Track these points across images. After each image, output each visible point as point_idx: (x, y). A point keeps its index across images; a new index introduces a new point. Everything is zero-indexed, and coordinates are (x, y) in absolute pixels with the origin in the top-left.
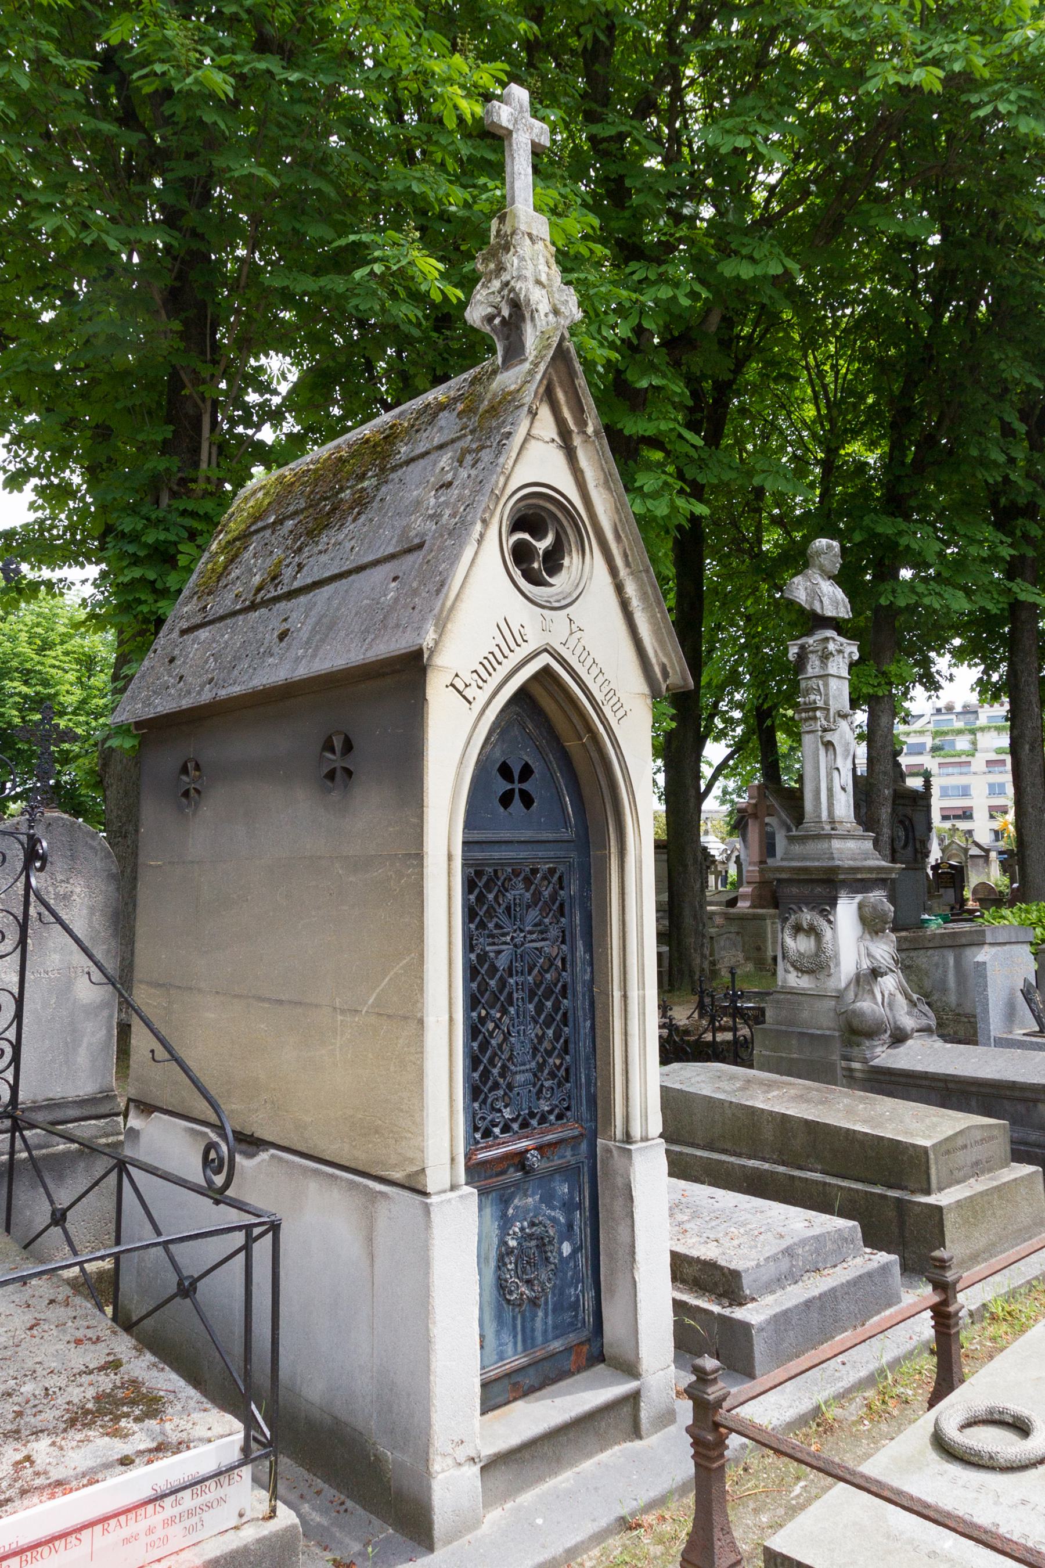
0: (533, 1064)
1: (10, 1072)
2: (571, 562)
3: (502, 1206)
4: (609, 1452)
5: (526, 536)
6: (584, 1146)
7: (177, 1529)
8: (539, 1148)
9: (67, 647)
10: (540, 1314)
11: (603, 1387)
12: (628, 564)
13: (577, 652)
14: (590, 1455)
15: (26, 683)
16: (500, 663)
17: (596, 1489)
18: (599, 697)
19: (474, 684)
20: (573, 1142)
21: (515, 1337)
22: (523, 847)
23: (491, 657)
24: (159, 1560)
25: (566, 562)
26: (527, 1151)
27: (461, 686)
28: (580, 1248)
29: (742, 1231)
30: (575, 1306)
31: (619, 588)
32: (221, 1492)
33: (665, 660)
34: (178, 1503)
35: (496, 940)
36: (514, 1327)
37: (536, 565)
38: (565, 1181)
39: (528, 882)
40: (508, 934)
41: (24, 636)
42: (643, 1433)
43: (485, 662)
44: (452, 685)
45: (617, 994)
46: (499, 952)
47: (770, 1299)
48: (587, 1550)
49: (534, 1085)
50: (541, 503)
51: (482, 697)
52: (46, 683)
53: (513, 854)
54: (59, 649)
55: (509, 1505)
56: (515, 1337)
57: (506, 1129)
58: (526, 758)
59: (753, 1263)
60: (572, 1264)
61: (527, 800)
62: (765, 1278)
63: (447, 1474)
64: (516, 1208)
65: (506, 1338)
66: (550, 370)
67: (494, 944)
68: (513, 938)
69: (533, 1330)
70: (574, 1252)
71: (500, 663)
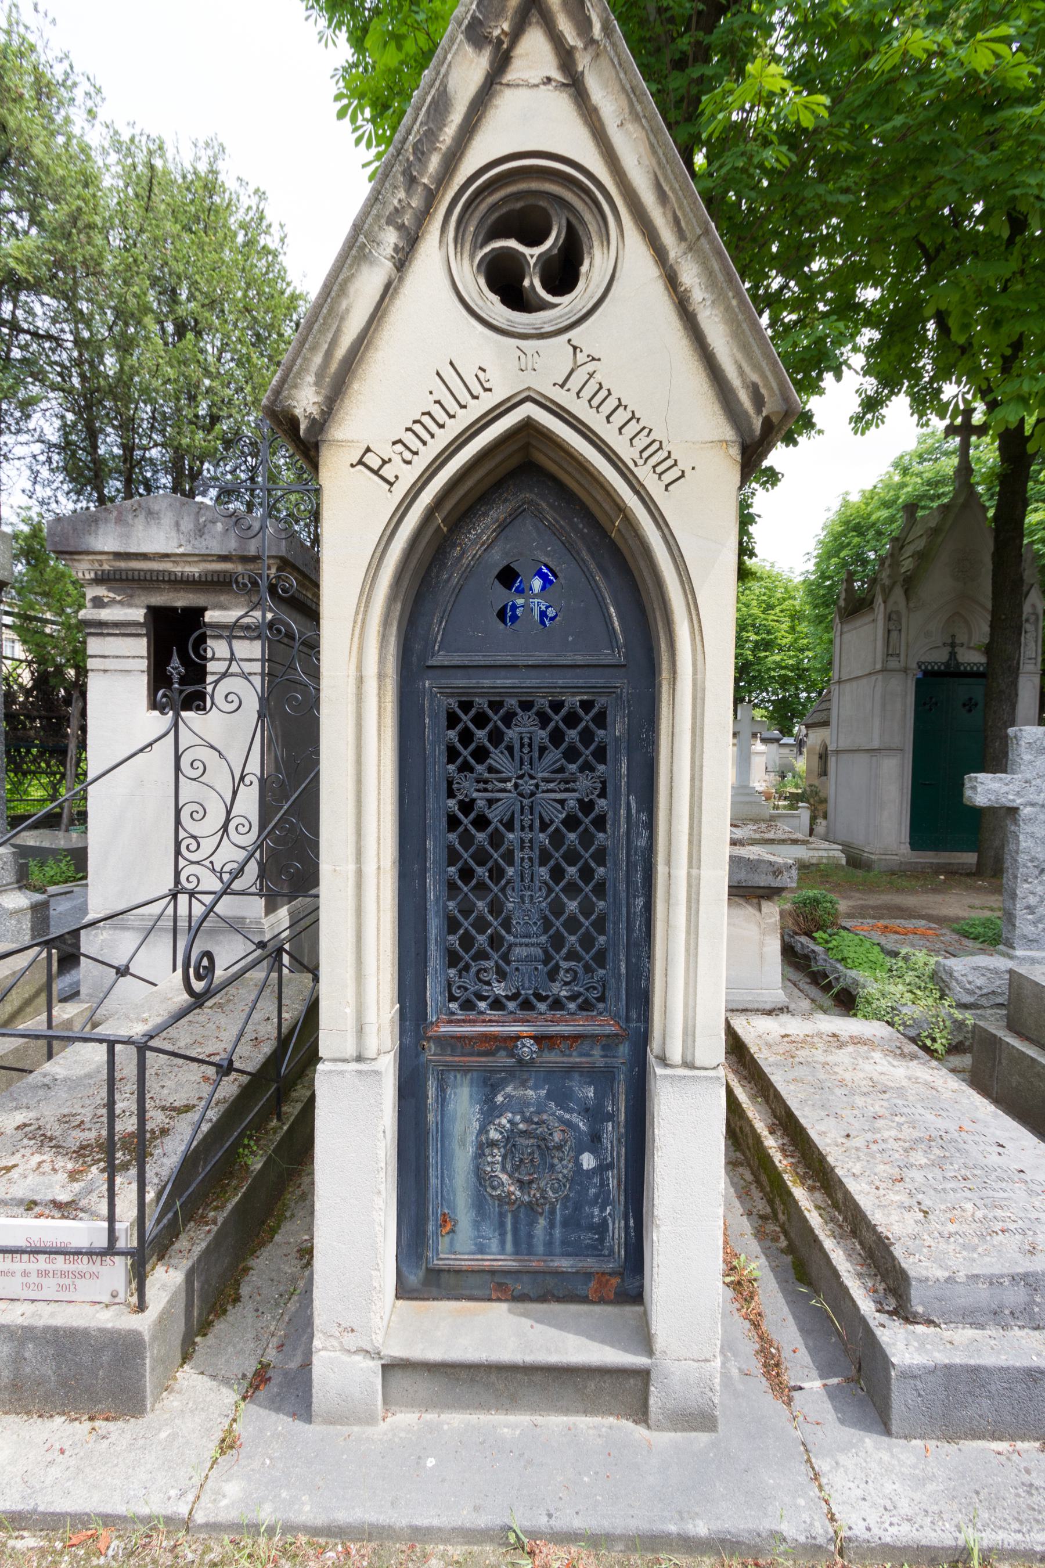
0: (543, 939)
1: (181, 865)
2: (595, 268)
3: (487, 1090)
4: (597, 1420)
5: (512, 243)
6: (624, 1050)
7: (50, 1283)
8: (538, 1039)
9: (784, 607)
10: (542, 1222)
11: (603, 1342)
12: (681, 236)
14: (567, 1411)
15: (757, 634)
17: (530, 1462)
18: (627, 453)
19: (396, 459)
20: (609, 1042)
21: (503, 1235)
22: (533, 672)
23: (426, 420)
24: (33, 1301)
26: (518, 1038)
28: (610, 1166)
29: (979, 1214)
30: (602, 1228)
31: (671, 280)
32: (94, 1268)
33: (755, 377)
34: (51, 1262)
35: (489, 786)
36: (502, 1225)
38: (590, 1084)
39: (544, 720)
40: (509, 780)
41: (754, 603)
43: (417, 428)
44: (361, 462)
46: (490, 802)
47: (965, 1334)
48: (447, 1541)
49: (545, 963)
51: (409, 475)
52: (769, 633)
53: (516, 682)
54: (778, 609)
55: (430, 1417)
56: (503, 1235)
57: (497, 1004)
59: (942, 1274)
60: (596, 1180)
62: (961, 1302)
63: (332, 1354)
64: (508, 1096)
65: (487, 1230)
67: (486, 790)
68: (516, 786)
69: (530, 1236)
70: (602, 1168)
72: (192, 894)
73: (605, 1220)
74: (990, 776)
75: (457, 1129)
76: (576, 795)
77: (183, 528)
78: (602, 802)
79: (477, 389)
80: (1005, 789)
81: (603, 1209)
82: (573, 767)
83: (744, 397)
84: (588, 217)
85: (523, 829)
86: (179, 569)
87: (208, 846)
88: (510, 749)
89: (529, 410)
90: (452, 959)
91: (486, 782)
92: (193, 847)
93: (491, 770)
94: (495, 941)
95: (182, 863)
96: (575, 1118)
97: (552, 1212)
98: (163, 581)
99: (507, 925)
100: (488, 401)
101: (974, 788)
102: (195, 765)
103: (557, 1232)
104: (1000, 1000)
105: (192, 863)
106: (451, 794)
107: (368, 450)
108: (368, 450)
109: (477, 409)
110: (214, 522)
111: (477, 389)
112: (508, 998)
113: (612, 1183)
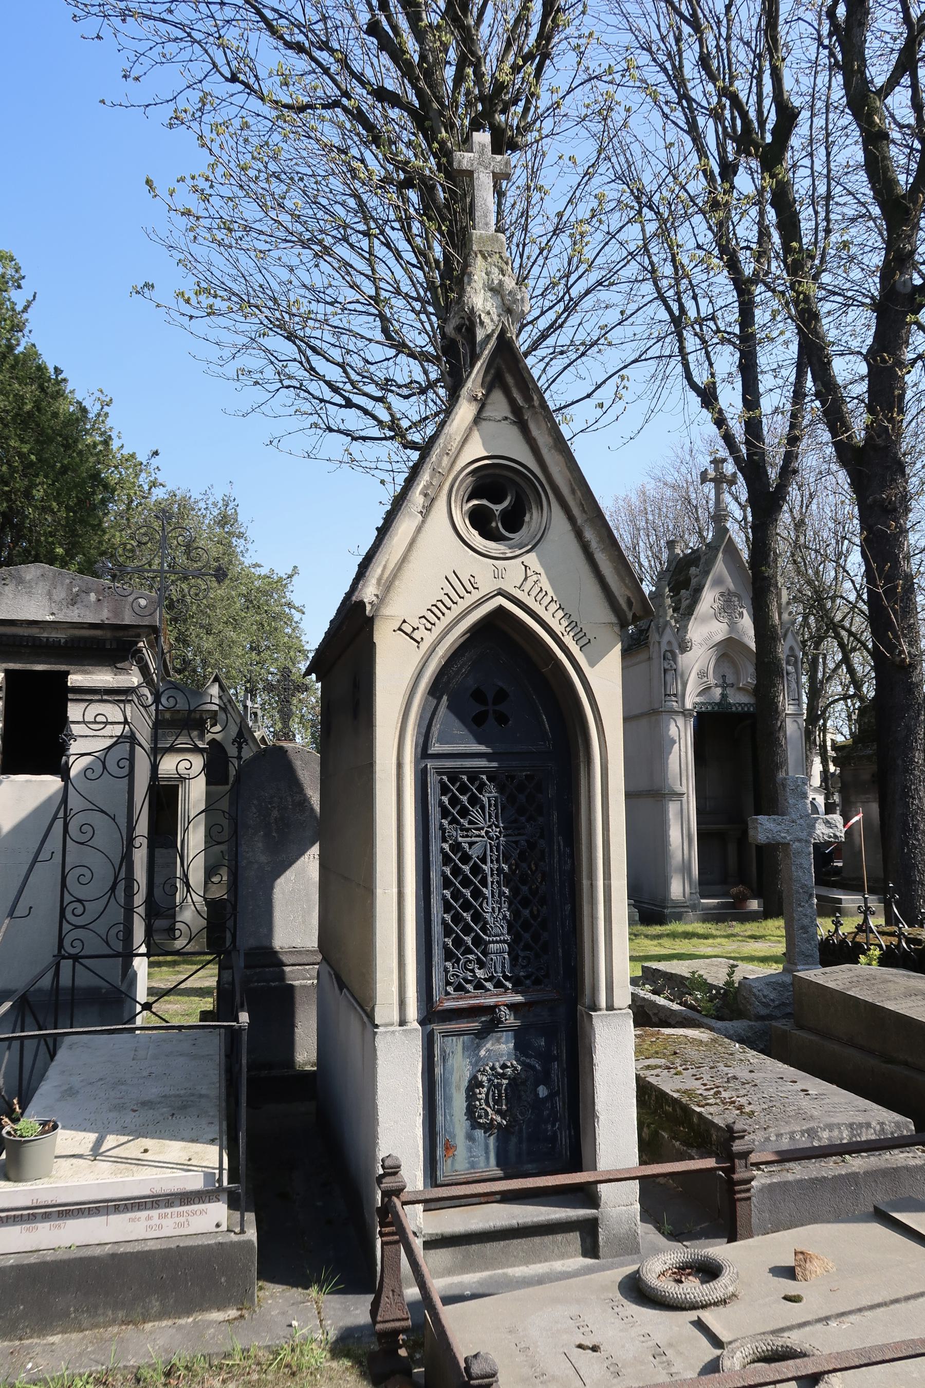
5: (485, 502)
13: (533, 593)
16: (449, 609)
19: (422, 628)
23: (440, 605)
25: (527, 518)
27: (408, 629)
28: (557, 1093)
30: (553, 1139)
31: (579, 534)
35: (470, 834)
37: (494, 524)
40: (482, 828)
42: (601, 1254)
43: (434, 609)
44: (400, 629)
45: (585, 882)
50: (497, 471)
51: (429, 638)
57: (479, 986)
58: (500, 684)
60: (549, 1105)
61: (502, 719)
64: (488, 1050)
66: (498, 360)
67: (467, 836)
68: (487, 832)
70: (551, 1096)
71: (449, 609)
72: (76, 958)
73: (555, 1133)
74: (766, 817)
75: (455, 1078)
76: (524, 837)
77: (55, 597)
78: (542, 842)
79: (470, 588)
80: (779, 828)
81: (553, 1125)
82: (523, 819)
83: (624, 606)
84: (528, 491)
85: (492, 862)
86: (45, 635)
87: (93, 908)
88: (483, 808)
89: (501, 601)
90: (449, 955)
91: (467, 830)
92: (79, 911)
93: (471, 822)
94: (477, 941)
95: (67, 927)
96: (533, 1062)
97: (521, 1130)
98: (27, 646)
99: (484, 929)
100: (476, 595)
101: (756, 828)
102: (84, 828)
103: (524, 1146)
104: (789, 1010)
105: (77, 927)
106: (444, 840)
107: (404, 621)
108: (404, 621)
109: (470, 599)
110: (87, 593)
111: (470, 588)
112: (486, 980)
113: (559, 1104)
